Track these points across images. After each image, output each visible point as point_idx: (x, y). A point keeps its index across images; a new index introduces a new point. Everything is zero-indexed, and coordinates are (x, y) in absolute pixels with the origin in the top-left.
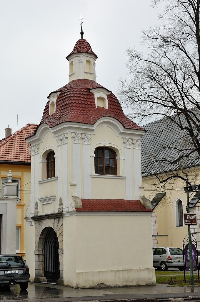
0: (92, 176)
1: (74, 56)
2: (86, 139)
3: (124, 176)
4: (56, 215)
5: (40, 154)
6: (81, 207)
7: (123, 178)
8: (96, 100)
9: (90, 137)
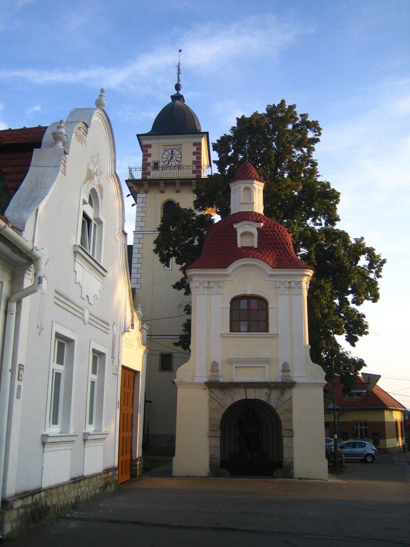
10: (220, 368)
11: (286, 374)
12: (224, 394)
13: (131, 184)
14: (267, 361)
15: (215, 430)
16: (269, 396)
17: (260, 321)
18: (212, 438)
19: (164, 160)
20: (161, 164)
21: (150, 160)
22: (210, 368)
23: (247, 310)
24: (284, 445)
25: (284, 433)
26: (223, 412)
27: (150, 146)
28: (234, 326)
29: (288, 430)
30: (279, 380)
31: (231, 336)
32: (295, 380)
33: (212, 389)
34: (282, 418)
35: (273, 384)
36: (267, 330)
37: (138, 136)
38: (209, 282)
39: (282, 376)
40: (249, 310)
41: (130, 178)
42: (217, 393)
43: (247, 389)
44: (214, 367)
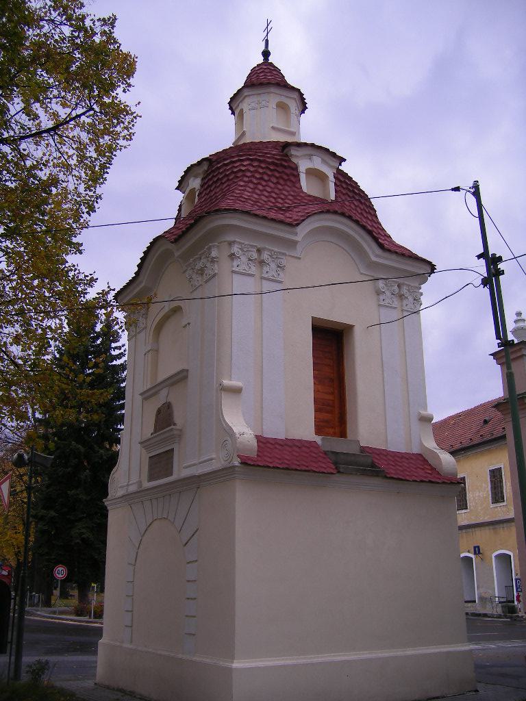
1: (243, 96)
2: (273, 266)
5: (148, 329)
6: (254, 454)
8: (303, 177)
9: (284, 262)
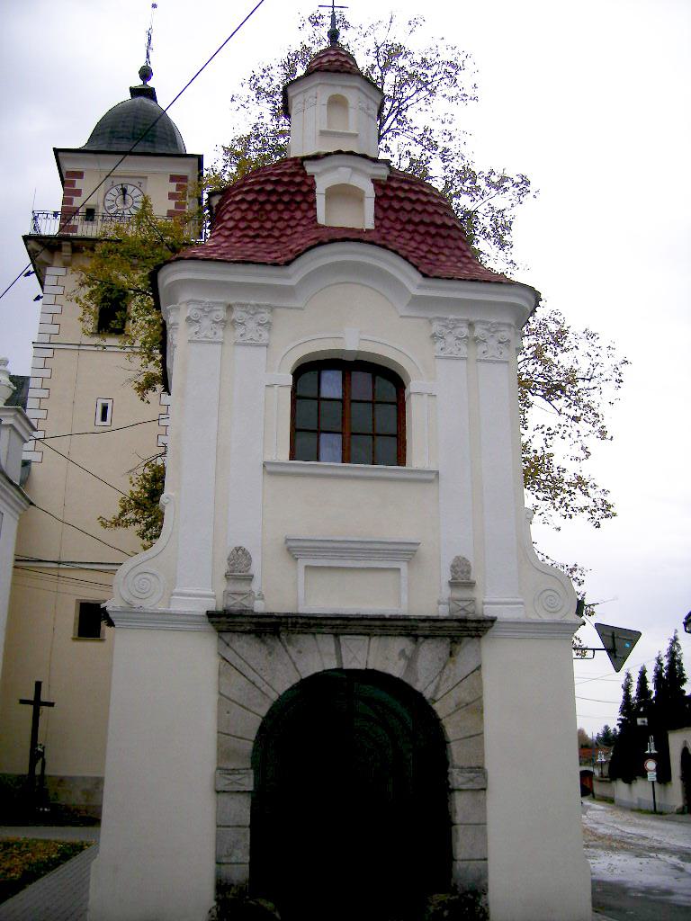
0: (269, 468)
3: (433, 468)
4: (338, 622)
7: (430, 478)
10: (255, 569)
11: (459, 594)
12: (270, 654)
13: (33, 244)
14: (407, 552)
15: (233, 771)
16: (411, 661)
17: (370, 435)
18: (224, 797)
19: (108, 204)
20: (101, 210)
21: (77, 202)
22: (224, 568)
23: (342, 401)
24: (458, 818)
25: (457, 778)
26: (264, 711)
27: (80, 175)
28: (304, 439)
29: (471, 769)
30: (443, 612)
31: (293, 470)
32: (489, 612)
33: (227, 637)
34: (451, 732)
35: (427, 624)
36: (400, 458)
37: (57, 151)
38: (229, 308)
39: (452, 600)
40: (345, 402)
41: (33, 232)
42: (247, 648)
43: (342, 638)
44: (238, 568)
